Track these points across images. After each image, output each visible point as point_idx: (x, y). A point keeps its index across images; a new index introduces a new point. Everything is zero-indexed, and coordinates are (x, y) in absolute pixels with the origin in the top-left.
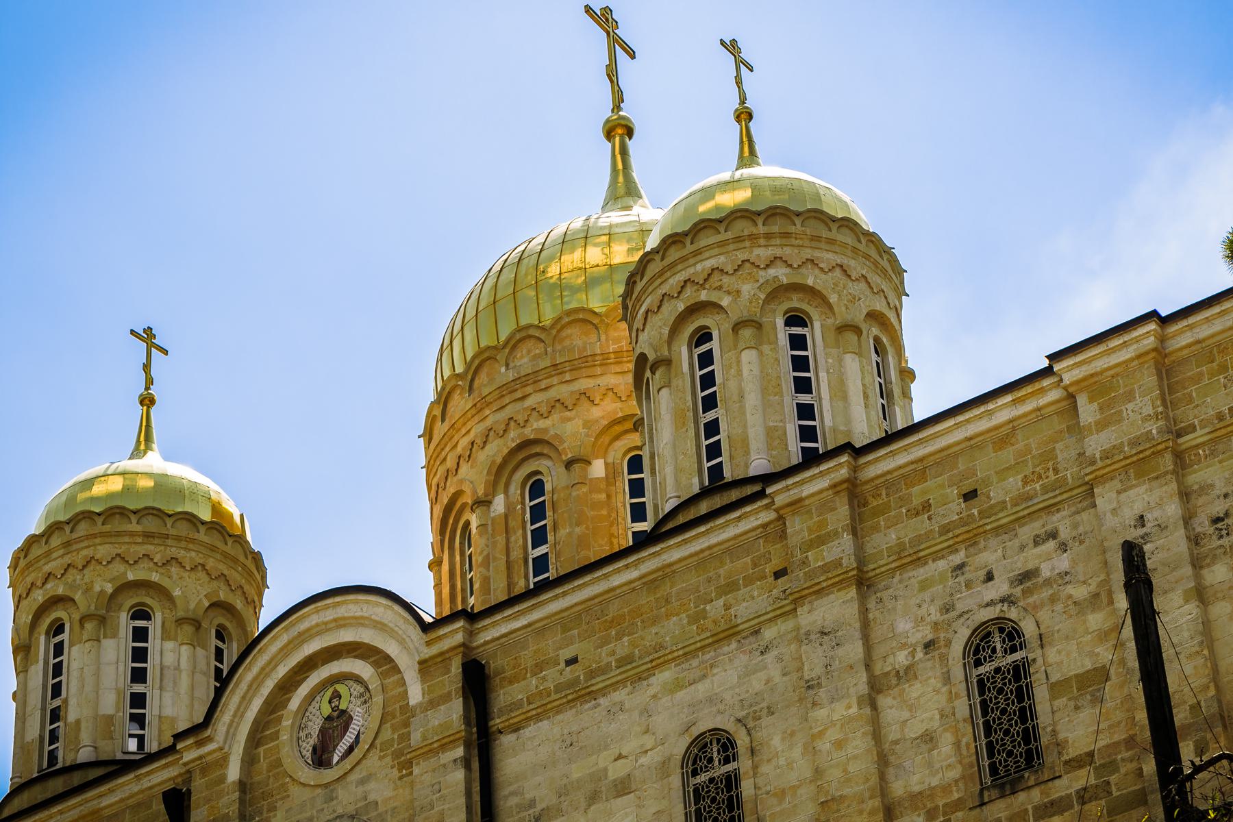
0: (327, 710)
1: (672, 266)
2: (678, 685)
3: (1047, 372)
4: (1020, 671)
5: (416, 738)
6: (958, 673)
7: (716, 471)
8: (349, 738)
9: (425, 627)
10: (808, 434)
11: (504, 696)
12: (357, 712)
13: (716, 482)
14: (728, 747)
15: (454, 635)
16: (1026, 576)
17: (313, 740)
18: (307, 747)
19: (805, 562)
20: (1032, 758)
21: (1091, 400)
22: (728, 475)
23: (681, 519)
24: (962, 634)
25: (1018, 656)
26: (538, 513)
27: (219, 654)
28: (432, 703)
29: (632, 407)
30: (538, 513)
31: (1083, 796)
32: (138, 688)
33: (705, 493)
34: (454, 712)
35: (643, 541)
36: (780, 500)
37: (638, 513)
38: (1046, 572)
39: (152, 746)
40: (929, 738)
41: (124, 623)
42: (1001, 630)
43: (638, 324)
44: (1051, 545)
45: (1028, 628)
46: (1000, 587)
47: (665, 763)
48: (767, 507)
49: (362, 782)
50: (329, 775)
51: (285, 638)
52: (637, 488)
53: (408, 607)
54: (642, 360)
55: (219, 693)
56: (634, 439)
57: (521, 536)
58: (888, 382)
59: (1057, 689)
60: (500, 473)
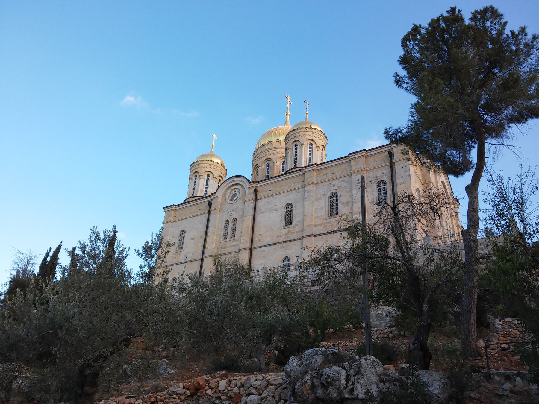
0: (233, 193)
1: (293, 134)
2: (285, 196)
3: (347, 156)
4: (337, 200)
5: (246, 199)
6: (327, 199)
7: (295, 165)
8: (236, 198)
9: (250, 182)
10: (310, 162)
12: (238, 194)
13: (295, 167)
14: (292, 206)
15: (255, 184)
16: (339, 187)
17: (231, 197)
18: (230, 198)
19: (307, 180)
22: (297, 166)
23: (289, 172)
24: (329, 194)
25: (337, 198)
26: (268, 169)
27: (219, 183)
28: (249, 194)
29: (284, 155)
30: (268, 169)
32: (207, 186)
33: (293, 168)
35: (283, 175)
36: (304, 171)
37: (283, 171)
38: (343, 186)
39: (208, 195)
40: (322, 208)
42: (383, 182)
43: (287, 142)
44: (344, 182)
45: (339, 194)
46: (336, 187)
47: (282, 207)
48: (348, 158)
49: (238, 204)
50: (232, 202)
51: (230, 181)
52: (283, 167)
53: (248, 180)
54: (286, 148)
55: (218, 188)
56: (284, 160)
57: (265, 172)
58: (323, 156)
59: (342, 204)
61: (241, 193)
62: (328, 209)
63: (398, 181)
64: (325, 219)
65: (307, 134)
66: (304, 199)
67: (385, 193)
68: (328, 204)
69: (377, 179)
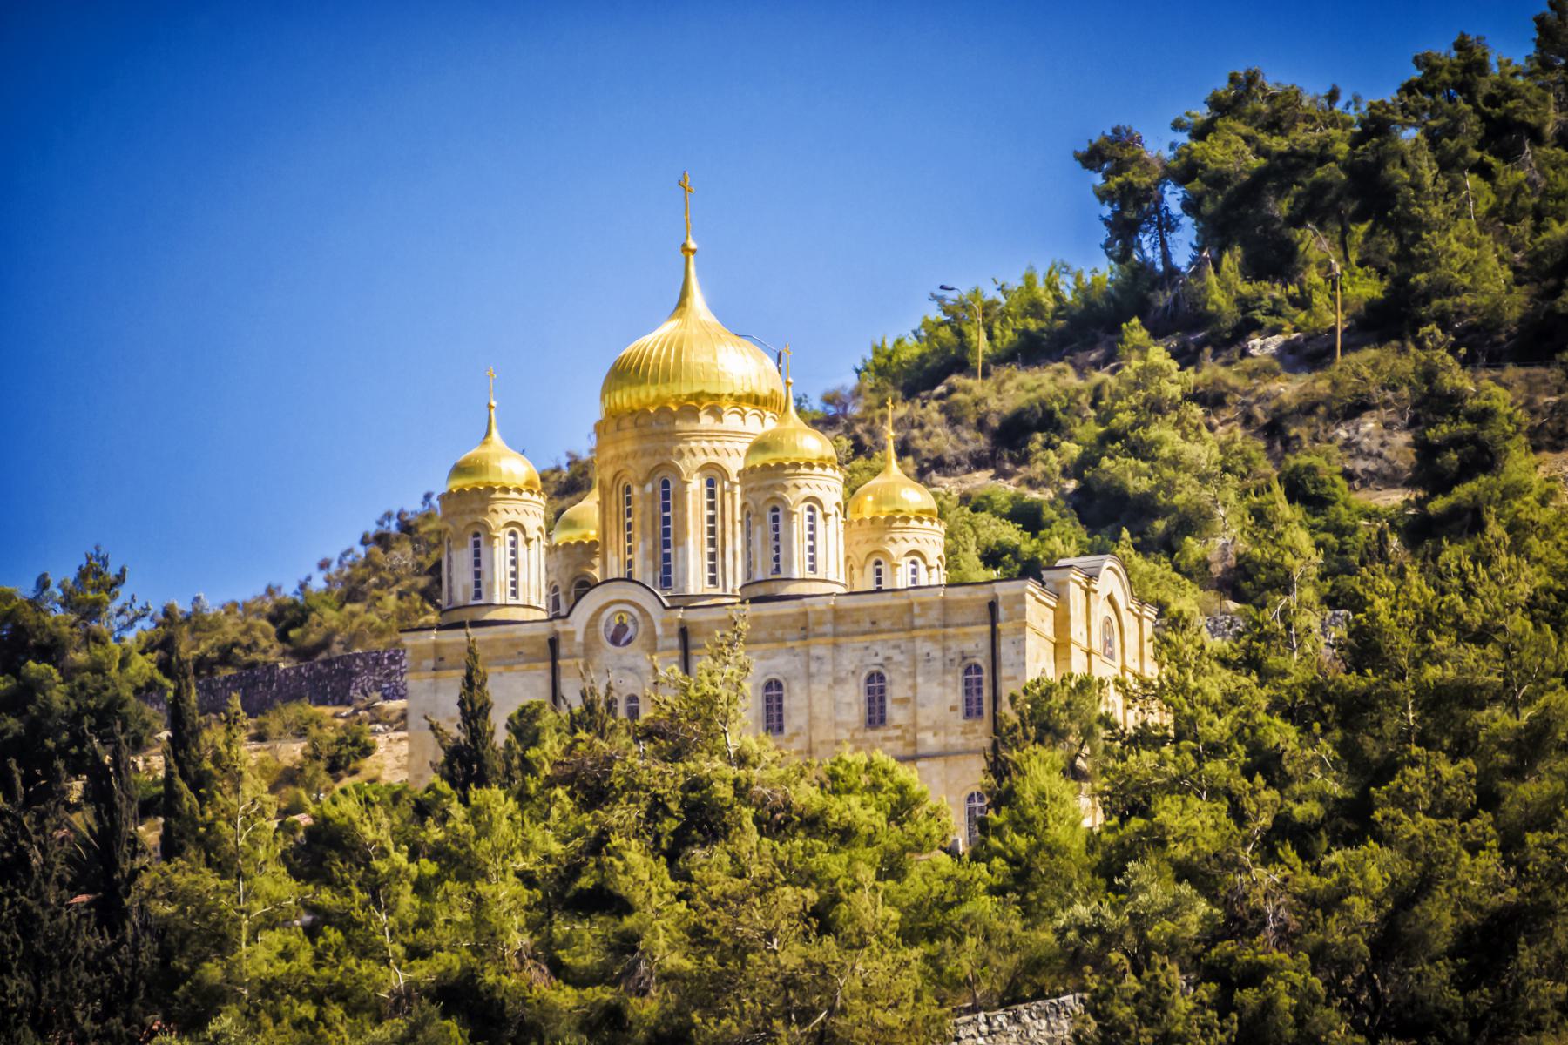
4: (882, 690)
11: (693, 641)
14: (779, 686)
16: (888, 659)
18: (610, 634)
20: (882, 720)
21: (573, 633)
26: (666, 496)
31: (898, 738)
34: (676, 642)
41: (470, 541)
46: (879, 660)
59: (895, 701)
60: (651, 474)
61: (641, 626)
62: (864, 708)
63: (1005, 672)
64: (857, 730)
65: (801, 482)
66: (810, 676)
67: (979, 691)
68: (863, 697)
69: (964, 658)
